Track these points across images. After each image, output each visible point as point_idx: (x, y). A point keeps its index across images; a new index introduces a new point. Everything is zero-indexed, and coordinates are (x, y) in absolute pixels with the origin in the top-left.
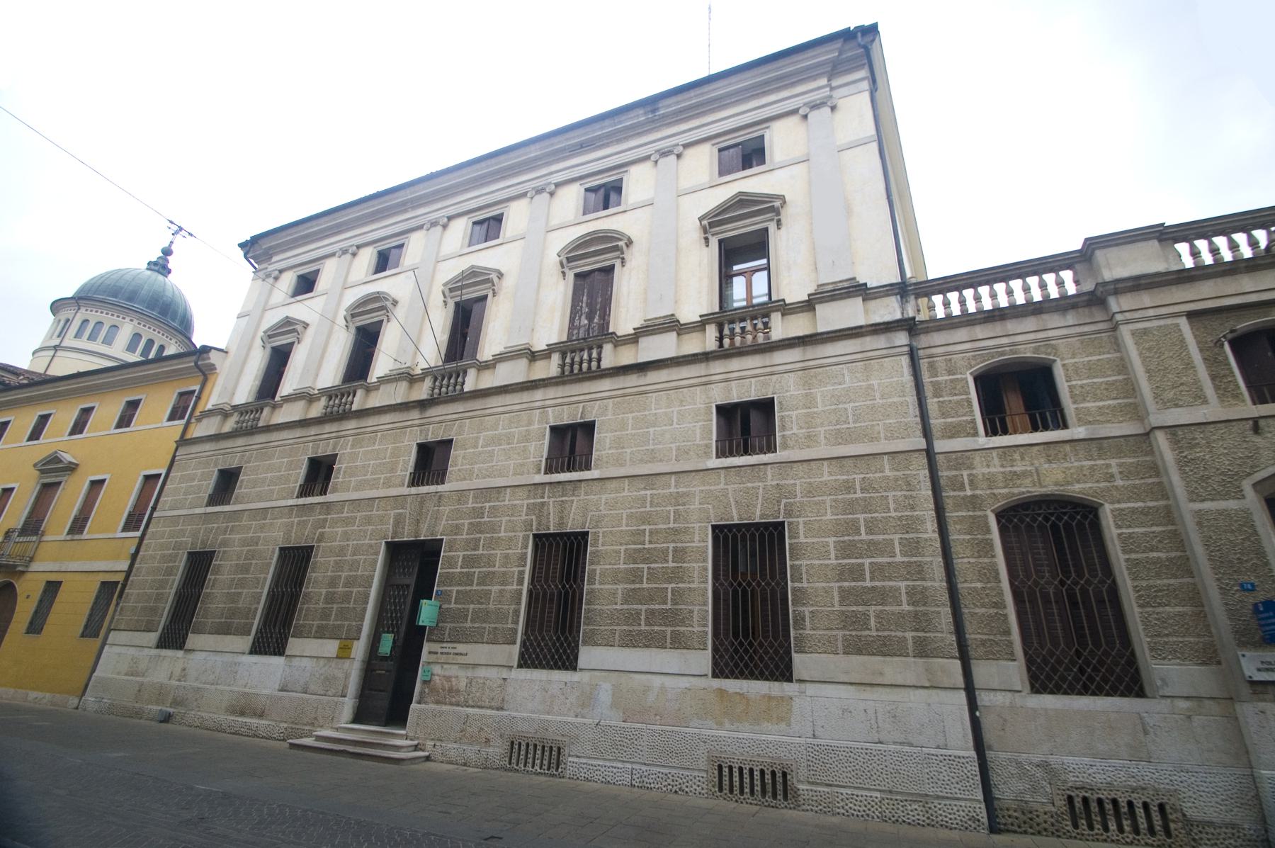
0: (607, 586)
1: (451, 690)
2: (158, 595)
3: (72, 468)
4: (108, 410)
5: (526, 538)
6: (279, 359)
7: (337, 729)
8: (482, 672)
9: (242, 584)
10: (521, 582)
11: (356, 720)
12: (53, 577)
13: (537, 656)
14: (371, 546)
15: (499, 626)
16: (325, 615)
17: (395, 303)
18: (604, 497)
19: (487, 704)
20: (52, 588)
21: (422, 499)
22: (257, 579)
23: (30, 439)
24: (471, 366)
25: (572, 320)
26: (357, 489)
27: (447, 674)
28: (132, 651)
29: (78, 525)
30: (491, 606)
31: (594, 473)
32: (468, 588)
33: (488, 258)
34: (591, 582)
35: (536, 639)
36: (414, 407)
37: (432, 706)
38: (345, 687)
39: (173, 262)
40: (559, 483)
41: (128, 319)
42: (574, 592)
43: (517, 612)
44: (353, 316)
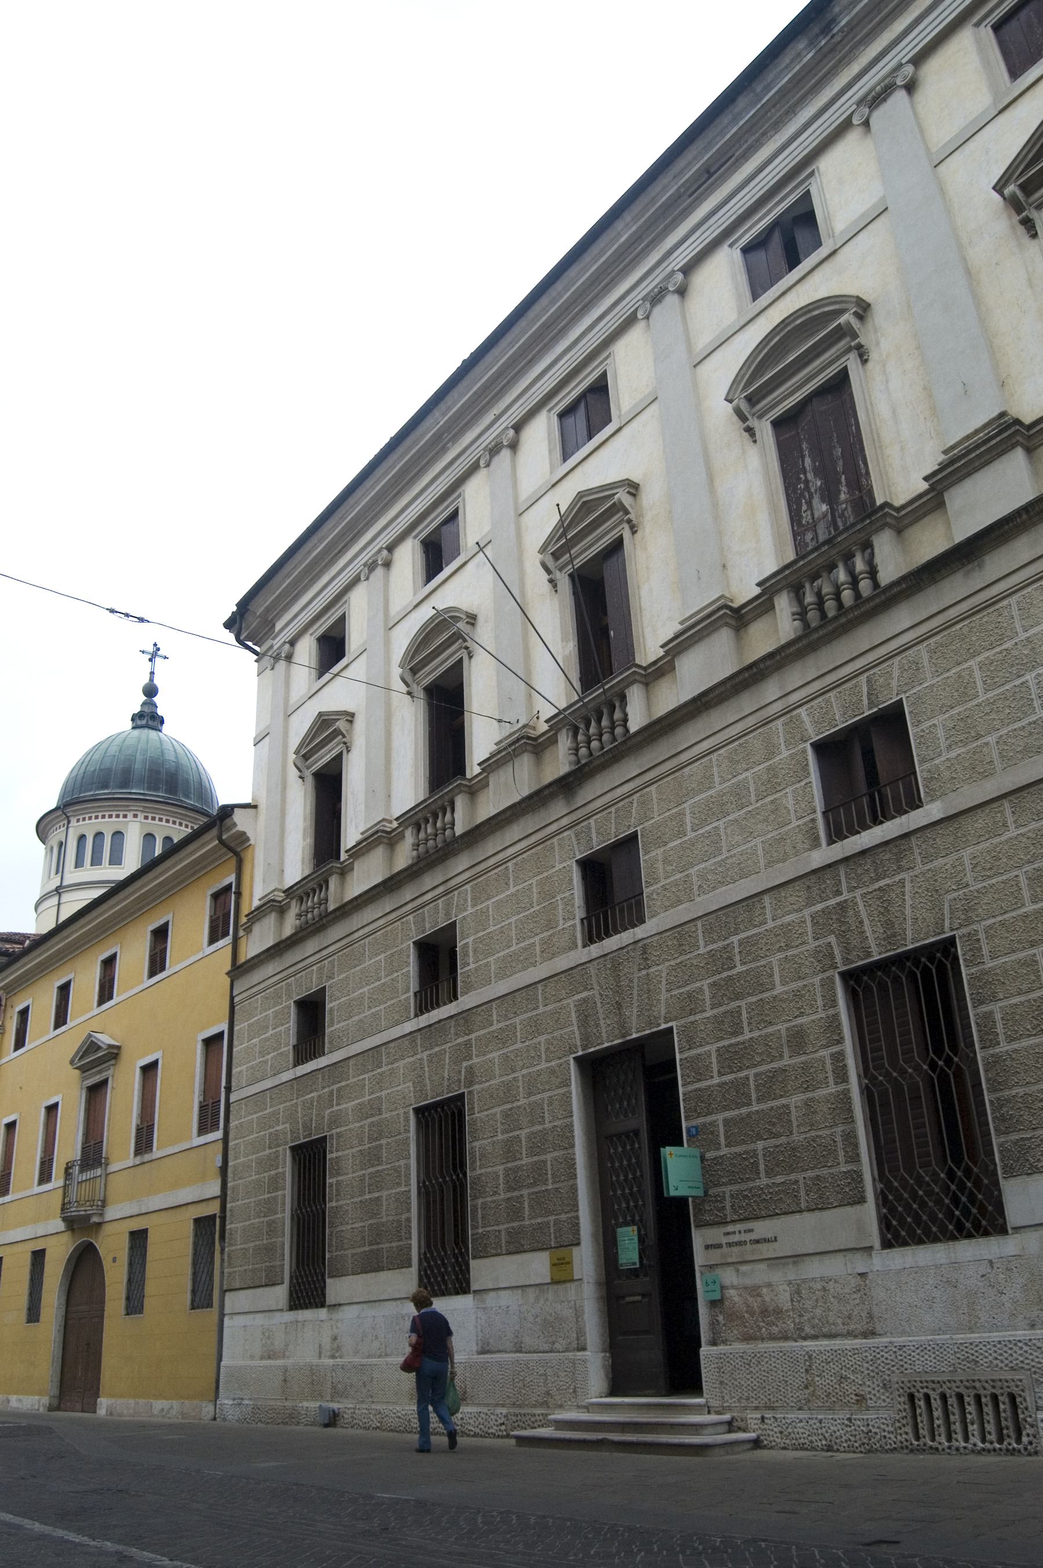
0: (1025, 1043)
1: (764, 1312)
2: (270, 1224)
3: (114, 1054)
4: (133, 951)
5: (828, 985)
6: (328, 787)
7: (588, 1408)
8: (814, 1269)
9: (377, 1182)
10: (842, 1076)
11: (615, 1390)
12: (136, 1225)
13: (917, 1220)
14: (552, 1071)
15: (825, 1172)
16: (514, 1212)
17: (472, 619)
18: (966, 854)
19: (841, 1328)
20: (139, 1239)
21: (613, 961)
22: (396, 1170)
23: (100, 1003)
24: (629, 682)
25: (795, 517)
26: (503, 973)
27: (748, 1282)
28: (259, 1320)
29: (144, 1141)
30: (797, 1137)
31: (932, 811)
32: (744, 1110)
33: (602, 467)
34: (989, 1042)
35: (904, 1184)
36: (553, 796)
37: (739, 1347)
38: (581, 1333)
39: (163, 705)
40: (863, 853)
41: (130, 815)
42: (959, 1074)
43: (850, 1139)
44: (414, 671)
